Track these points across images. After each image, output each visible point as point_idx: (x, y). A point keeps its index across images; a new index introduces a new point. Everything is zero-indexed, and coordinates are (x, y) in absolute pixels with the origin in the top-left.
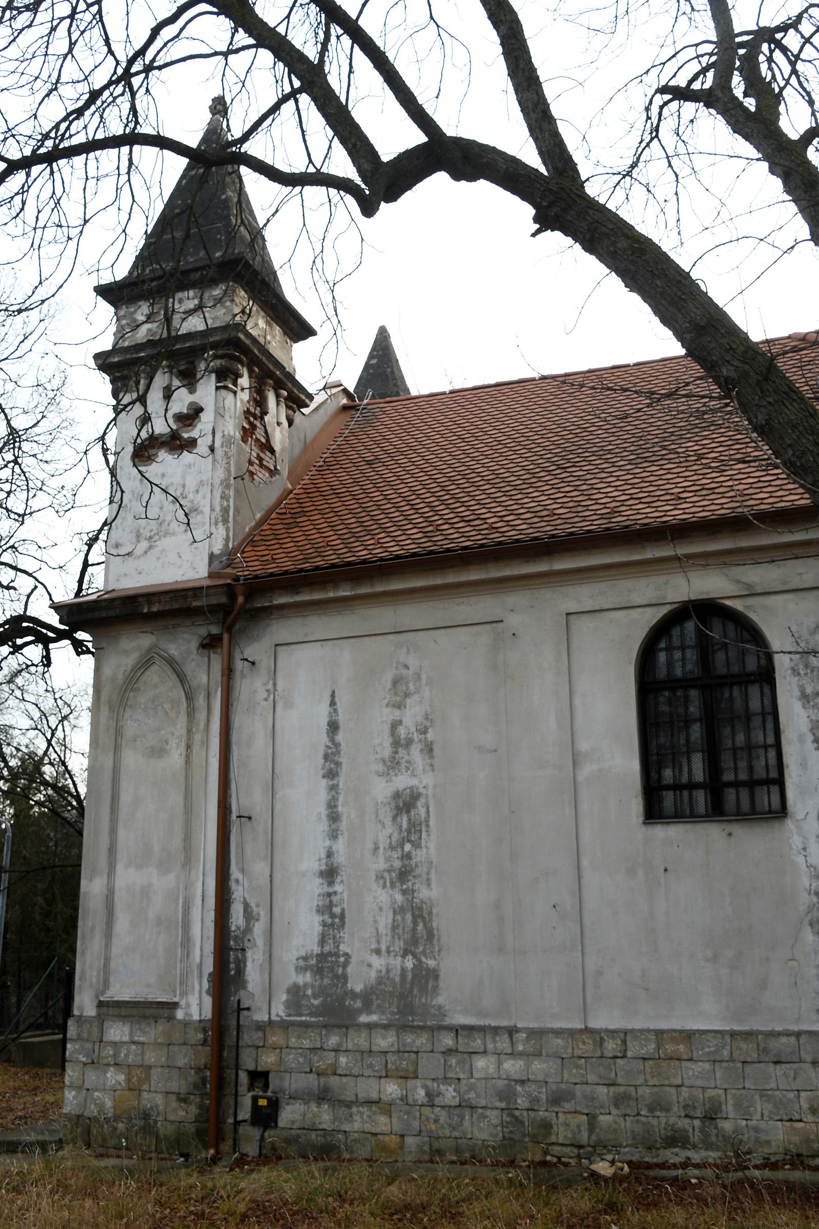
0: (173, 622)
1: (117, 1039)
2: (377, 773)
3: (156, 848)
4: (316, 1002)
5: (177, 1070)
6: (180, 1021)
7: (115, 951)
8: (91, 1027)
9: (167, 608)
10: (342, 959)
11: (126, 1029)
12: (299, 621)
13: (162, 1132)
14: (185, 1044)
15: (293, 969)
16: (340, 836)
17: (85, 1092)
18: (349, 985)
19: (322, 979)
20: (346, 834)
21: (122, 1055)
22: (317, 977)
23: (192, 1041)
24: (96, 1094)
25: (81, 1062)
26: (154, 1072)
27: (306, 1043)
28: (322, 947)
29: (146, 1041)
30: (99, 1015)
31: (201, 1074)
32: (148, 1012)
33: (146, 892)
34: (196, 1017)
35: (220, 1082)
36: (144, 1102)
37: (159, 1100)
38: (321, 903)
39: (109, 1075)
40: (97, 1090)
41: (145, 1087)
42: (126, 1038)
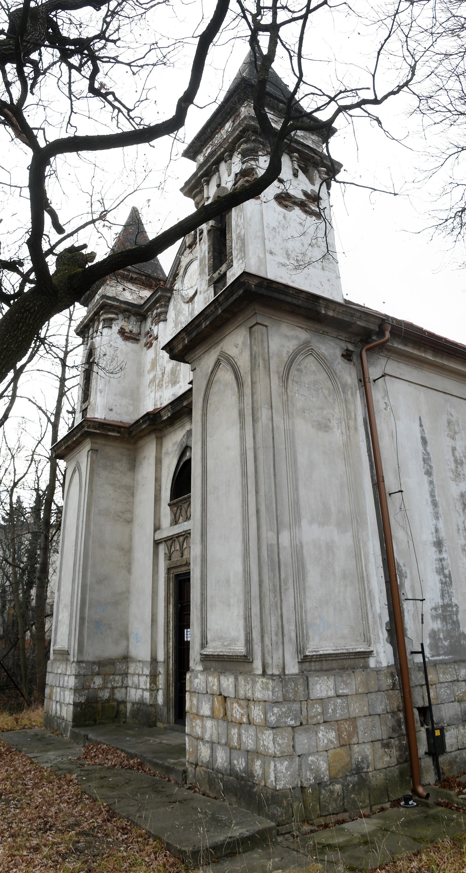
0: (325, 329)
1: (324, 695)
2: (451, 478)
3: (334, 509)
4: (446, 643)
5: (378, 716)
6: (373, 670)
7: (310, 604)
8: (296, 685)
9: (339, 317)
10: (454, 609)
11: (331, 683)
12: (396, 363)
13: (374, 782)
14: (379, 691)
15: (430, 618)
16: (440, 518)
17: (297, 759)
18: (461, 629)
19: (447, 625)
20: (443, 517)
21: (330, 711)
22: (444, 623)
23: (384, 687)
24: (310, 758)
25: (289, 726)
26: (360, 723)
27: (449, 678)
28: (443, 600)
29: (350, 693)
30: (302, 672)
31: (396, 717)
32: (346, 663)
33: (330, 547)
34: (385, 664)
35: (408, 721)
36: (356, 756)
37: (367, 749)
38: (438, 566)
39: (320, 735)
40: (310, 754)
41: (355, 740)
42: (331, 693)
